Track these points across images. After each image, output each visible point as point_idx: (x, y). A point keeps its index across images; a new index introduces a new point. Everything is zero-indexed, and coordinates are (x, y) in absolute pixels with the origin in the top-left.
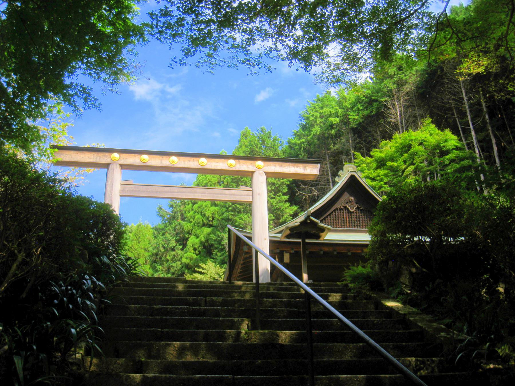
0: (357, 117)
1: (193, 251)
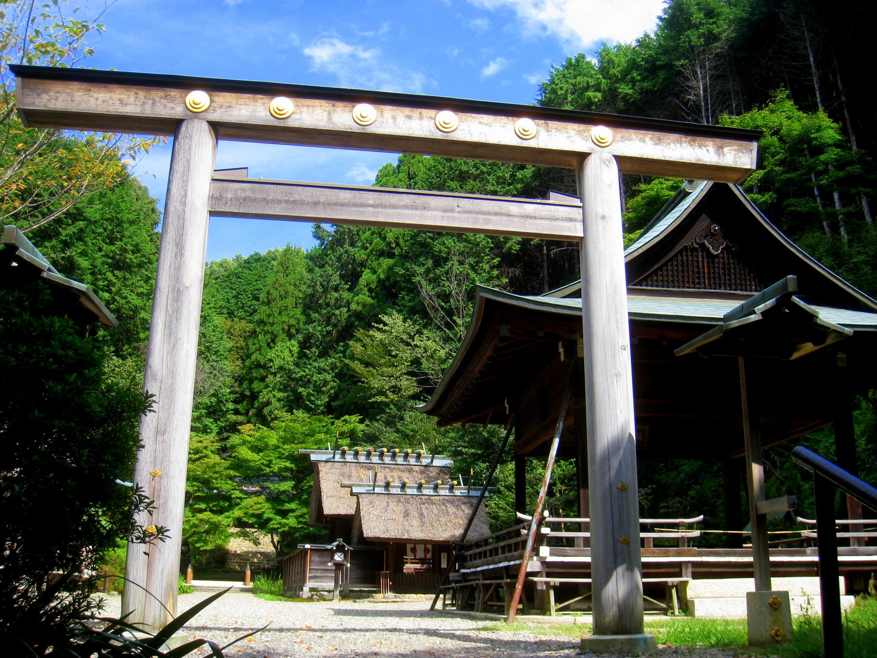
0: (630, 92)
1: (367, 293)
